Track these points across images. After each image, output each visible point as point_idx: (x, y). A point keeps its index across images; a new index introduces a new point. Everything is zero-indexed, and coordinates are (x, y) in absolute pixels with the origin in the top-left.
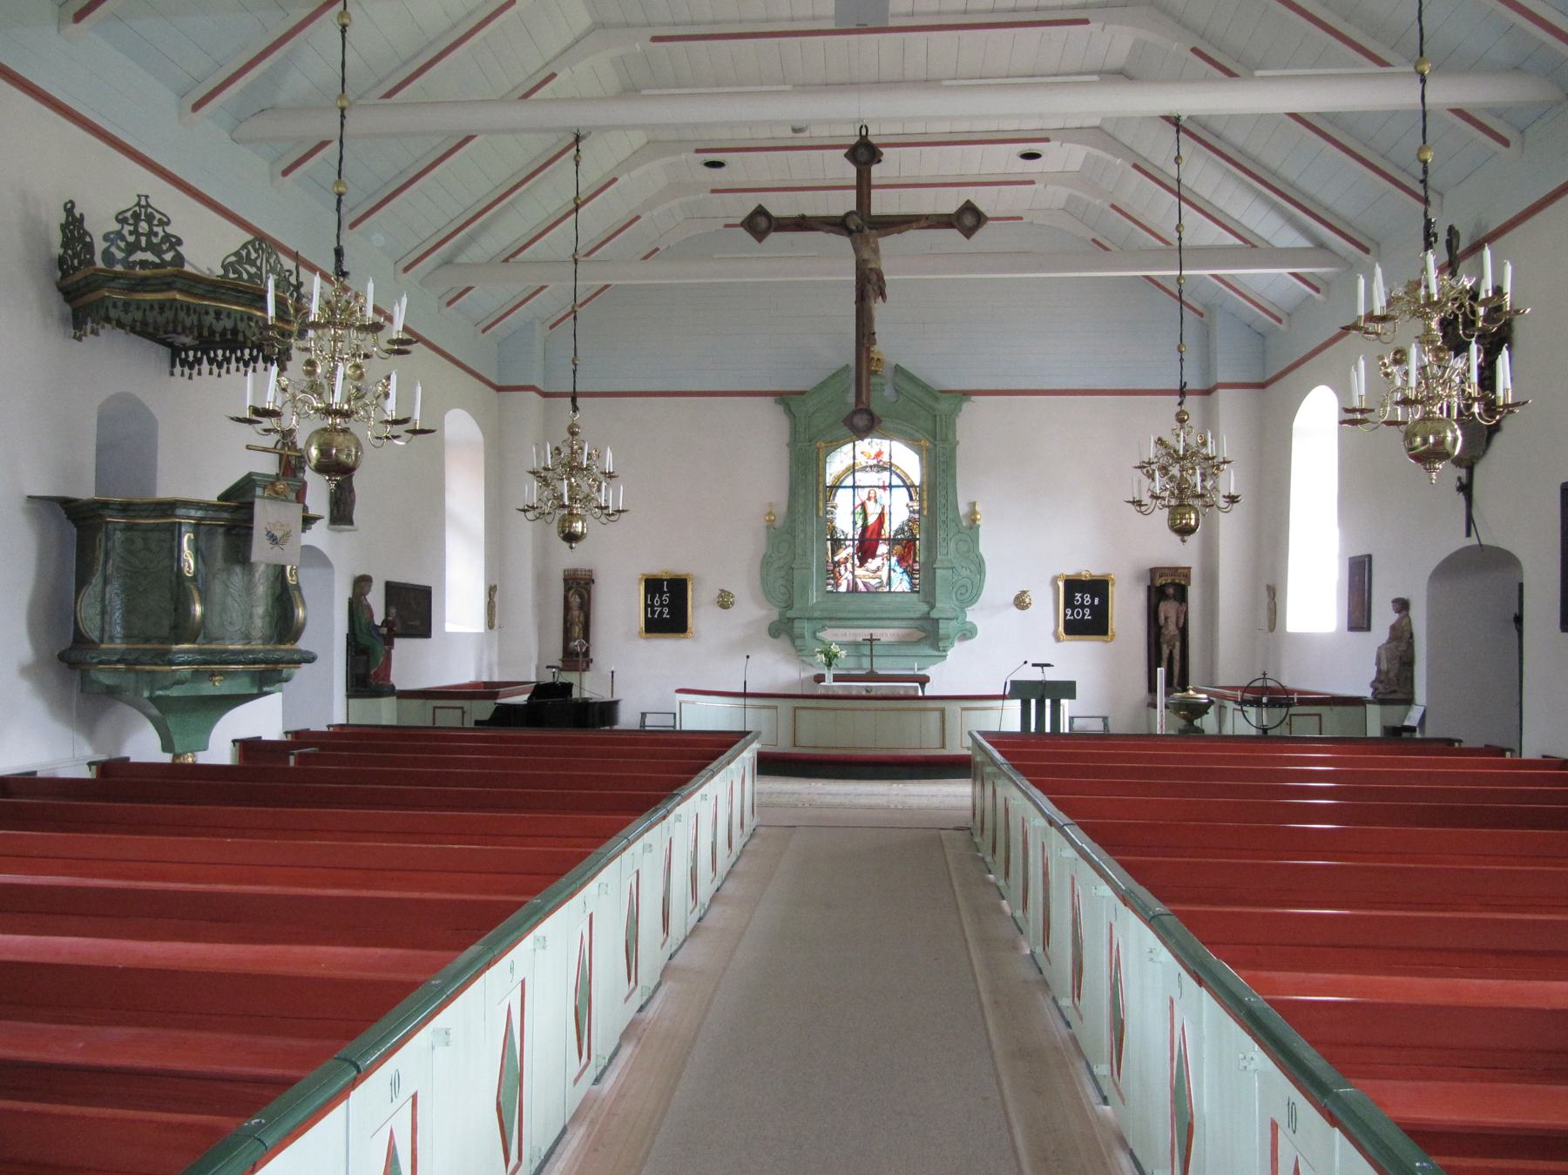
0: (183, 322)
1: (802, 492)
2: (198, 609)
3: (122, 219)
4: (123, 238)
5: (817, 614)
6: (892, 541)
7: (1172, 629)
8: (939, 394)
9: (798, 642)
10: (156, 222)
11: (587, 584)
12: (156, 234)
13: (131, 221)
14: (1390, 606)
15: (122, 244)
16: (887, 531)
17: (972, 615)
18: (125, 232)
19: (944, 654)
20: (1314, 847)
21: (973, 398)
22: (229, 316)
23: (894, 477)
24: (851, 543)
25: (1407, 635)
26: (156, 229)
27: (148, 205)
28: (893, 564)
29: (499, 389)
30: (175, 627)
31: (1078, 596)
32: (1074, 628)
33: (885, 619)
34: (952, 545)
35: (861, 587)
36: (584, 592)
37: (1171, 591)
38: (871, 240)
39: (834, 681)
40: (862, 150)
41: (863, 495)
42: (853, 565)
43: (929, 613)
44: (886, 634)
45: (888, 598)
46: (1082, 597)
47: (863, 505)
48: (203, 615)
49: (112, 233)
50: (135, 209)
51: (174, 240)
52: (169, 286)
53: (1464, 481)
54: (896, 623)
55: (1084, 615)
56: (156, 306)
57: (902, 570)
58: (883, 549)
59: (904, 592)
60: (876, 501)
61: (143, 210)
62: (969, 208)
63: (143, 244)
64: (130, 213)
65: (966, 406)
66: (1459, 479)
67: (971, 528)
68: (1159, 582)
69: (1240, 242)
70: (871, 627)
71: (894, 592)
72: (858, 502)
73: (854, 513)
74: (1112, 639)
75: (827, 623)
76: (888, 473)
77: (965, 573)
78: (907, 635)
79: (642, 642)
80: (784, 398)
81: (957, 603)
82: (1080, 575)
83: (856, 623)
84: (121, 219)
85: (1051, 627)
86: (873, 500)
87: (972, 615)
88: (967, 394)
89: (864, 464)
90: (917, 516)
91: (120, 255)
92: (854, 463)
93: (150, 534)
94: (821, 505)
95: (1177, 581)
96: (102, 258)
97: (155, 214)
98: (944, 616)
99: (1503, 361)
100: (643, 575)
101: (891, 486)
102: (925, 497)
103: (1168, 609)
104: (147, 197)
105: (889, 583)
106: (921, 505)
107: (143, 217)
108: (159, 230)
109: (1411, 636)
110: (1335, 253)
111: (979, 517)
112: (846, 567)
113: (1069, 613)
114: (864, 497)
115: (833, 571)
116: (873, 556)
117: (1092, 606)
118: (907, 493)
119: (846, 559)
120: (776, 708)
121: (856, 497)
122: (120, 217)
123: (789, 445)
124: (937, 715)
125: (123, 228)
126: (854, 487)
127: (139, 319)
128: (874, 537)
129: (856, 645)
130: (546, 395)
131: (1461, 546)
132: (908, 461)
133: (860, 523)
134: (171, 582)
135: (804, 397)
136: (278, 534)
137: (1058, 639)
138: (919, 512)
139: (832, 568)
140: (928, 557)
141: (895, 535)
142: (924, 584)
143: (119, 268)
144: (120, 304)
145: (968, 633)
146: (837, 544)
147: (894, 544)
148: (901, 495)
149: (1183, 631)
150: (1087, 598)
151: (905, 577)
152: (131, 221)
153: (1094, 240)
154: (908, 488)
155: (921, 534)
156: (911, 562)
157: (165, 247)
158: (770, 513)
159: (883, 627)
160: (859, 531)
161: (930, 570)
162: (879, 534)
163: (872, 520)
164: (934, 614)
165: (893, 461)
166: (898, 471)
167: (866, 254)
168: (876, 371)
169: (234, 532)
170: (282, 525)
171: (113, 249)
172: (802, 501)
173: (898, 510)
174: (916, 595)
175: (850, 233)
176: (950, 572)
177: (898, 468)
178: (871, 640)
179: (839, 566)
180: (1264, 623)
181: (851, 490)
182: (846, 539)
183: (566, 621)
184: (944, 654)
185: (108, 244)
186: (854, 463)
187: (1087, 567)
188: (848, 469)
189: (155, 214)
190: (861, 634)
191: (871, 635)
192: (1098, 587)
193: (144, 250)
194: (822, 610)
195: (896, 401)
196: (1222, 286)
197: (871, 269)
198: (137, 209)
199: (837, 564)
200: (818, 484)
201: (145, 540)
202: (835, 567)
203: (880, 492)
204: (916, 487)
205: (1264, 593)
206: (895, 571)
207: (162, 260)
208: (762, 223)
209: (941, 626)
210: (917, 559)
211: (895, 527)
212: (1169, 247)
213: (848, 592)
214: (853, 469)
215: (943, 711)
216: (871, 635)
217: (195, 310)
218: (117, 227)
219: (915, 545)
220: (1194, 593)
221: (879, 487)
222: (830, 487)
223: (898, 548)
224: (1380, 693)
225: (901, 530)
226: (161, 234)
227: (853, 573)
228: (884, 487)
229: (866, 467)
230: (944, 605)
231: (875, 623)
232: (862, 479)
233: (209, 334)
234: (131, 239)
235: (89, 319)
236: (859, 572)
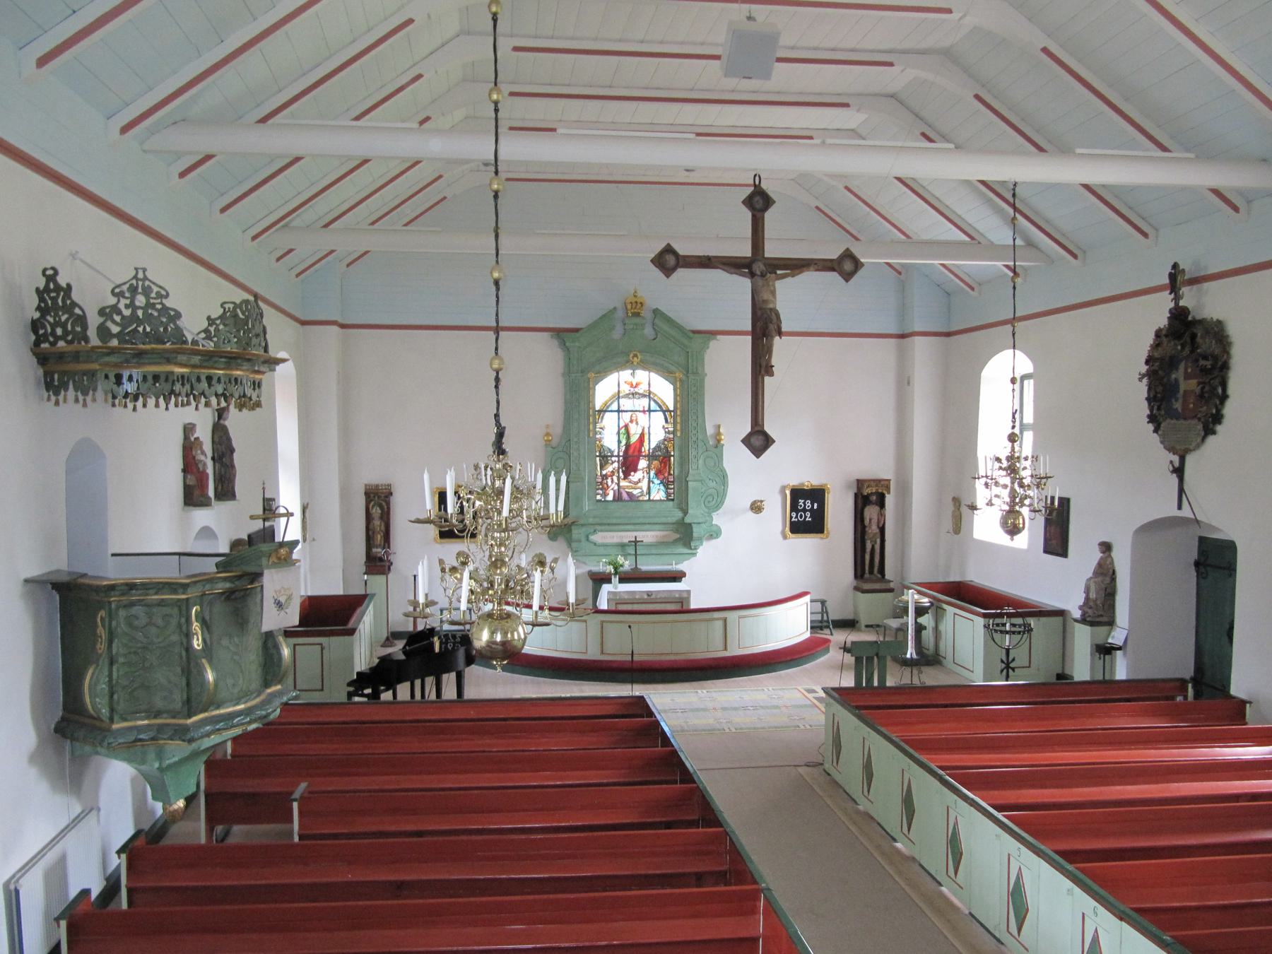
1: (576, 416)
2: (210, 676)
4: (119, 313)
5: (591, 520)
6: (651, 457)
7: (873, 529)
8: (691, 335)
9: (574, 545)
10: (153, 295)
11: (387, 497)
13: (127, 295)
14: (1097, 548)
15: (117, 318)
16: (647, 448)
17: (717, 519)
18: (121, 306)
19: (694, 552)
21: (719, 337)
23: (653, 404)
24: (617, 459)
25: (1111, 571)
27: (145, 278)
28: (652, 476)
29: (304, 323)
30: (188, 701)
31: (801, 502)
32: (797, 528)
33: (645, 524)
34: (701, 462)
35: (625, 496)
36: (384, 504)
37: (874, 498)
38: (771, 283)
40: (757, 198)
41: (626, 417)
42: (619, 478)
43: (683, 519)
44: (648, 536)
45: (649, 504)
46: (804, 503)
47: (626, 426)
48: (216, 681)
49: (108, 307)
50: (131, 282)
51: (172, 313)
52: (168, 358)
53: (1177, 464)
54: (657, 527)
55: (806, 517)
57: (659, 482)
58: (643, 463)
59: (661, 500)
60: (637, 423)
61: (140, 283)
62: (848, 255)
64: (127, 285)
65: (712, 344)
66: (1171, 462)
67: (716, 447)
68: (866, 491)
69: (967, 239)
70: (633, 531)
71: (653, 500)
72: (622, 424)
73: (618, 433)
74: (827, 537)
75: (597, 527)
76: (648, 400)
77: (712, 484)
78: (664, 536)
79: (438, 546)
80: (561, 334)
81: (706, 510)
82: (803, 484)
83: (622, 527)
85: (780, 527)
86: (634, 423)
87: (717, 519)
88: (714, 333)
89: (628, 392)
90: (671, 436)
91: (115, 329)
92: (619, 391)
93: (155, 610)
94: (591, 426)
95: (880, 491)
96: (98, 334)
97: (153, 286)
98: (695, 521)
100: (438, 488)
101: (650, 411)
102: (679, 420)
103: (871, 512)
104: (144, 270)
105: (649, 493)
106: (675, 427)
107: (140, 290)
109: (1114, 572)
110: (1042, 252)
111: (723, 437)
112: (612, 479)
113: (794, 516)
114: (627, 421)
115: (601, 483)
116: (635, 470)
117: (812, 510)
118: (663, 417)
119: (612, 472)
120: (585, 621)
121: (621, 420)
122: (117, 290)
123: (563, 375)
124: (719, 624)
125: (119, 301)
126: (619, 411)
128: (636, 453)
129: (622, 546)
130: (343, 326)
131: (1171, 515)
132: (665, 390)
133: (624, 442)
134: (181, 657)
135: (577, 335)
136: (282, 599)
137: (785, 537)
138: (674, 433)
139: (600, 480)
140: (681, 472)
141: (653, 452)
142: (679, 493)
143: (115, 343)
145: (714, 534)
146: (605, 458)
147: (653, 460)
148: (658, 418)
149: (882, 530)
150: (808, 503)
151: (662, 487)
152: (127, 295)
153: (817, 208)
154: (664, 412)
155: (676, 449)
156: (666, 475)
158: (548, 434)
159: (643, 531)
160: (623, 448)
161: (683, 481)
162: (640, 451)
163: (634, 439)
164: (687, 520)
165: (651, 390)
166: (655, 398)
167: (766, 296)
168: (639, 313)
169: (233, 597)
170: (285, 590)
171: (109, 324)
172: (576, 424)
173: (656, 430)
174: (671, 503)
175: (752, 275)
176: (699, 484)
177: (656, 395)
178: (636, 542)
179: (607, 478)
180: (948, 524)
181: (491, 335)
182: (612, 456)
183: (368, 529)
184: (694, 552)
186: (619, 391)
187: (808, 478)
188: (613, 397)
189: (153, 286)
190: (627, 537)
191: (636, 537)
192: (817, 495)
194: (594, 517)
195: (654, 339)
196: (946, 272)
197: (771, 309)
198: (134, 282)
199: (605, 477)
200: (589, 408)
201: (150, 615)
202: (603, 479)
203: (640, 415)
204: (670, 411)
205: (950, 507)
206: (653, 483)
208: (671, 260)
209: (694, 530)
210: (672, 472)
211: (653, 445)
212: (909, 240)
213: (614, 500)
214: (618, 396)
215: (725, 620)
216: (636, 537)
218: (113, 301)
219: (670, 460)
220: (890, 500)
221: (639, 411)
222: (598, 411)
223: (656, 463)
224: (1089, 616)
225: (658, 448)
227: (618, 484)
228: (644, 411)
229: (629, 394)
230: (695, 514)
231: (637, 527)
232: (626, 404)
234: (127, 313)
236: (623, 483)
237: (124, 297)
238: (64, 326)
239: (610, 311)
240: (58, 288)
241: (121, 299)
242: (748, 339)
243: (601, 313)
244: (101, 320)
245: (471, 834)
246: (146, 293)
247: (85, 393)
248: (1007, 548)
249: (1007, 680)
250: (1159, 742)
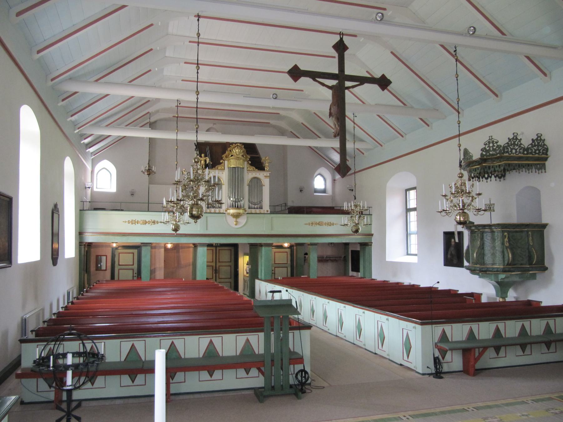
12: (495, 146)
18: (486, 147)
20: (104, 283)
22: (512, 165)
26: (494, 145)
27: (492, 139)
39: (352, 251)
56: (517, 165)
63: (491, 150)
84: (485, 144)
99: (273, 367)
104: (492, 136)
107: (491, 142)
108: (495, 145)
125: (485, 146)
144: (487, 167)
152: (488, 144)
157: (497, 149)
189: (494, 140)
207: (496, 153)
217: (522, 165)
218: (484, 146)
235: (207, 168)
237: (487, 145)
238: (516, 150)
240: (541, 139)
242: (301, 331)
244: (482, 152)
246: (493, 142)
247: (539, 170)
249: (162, 215)
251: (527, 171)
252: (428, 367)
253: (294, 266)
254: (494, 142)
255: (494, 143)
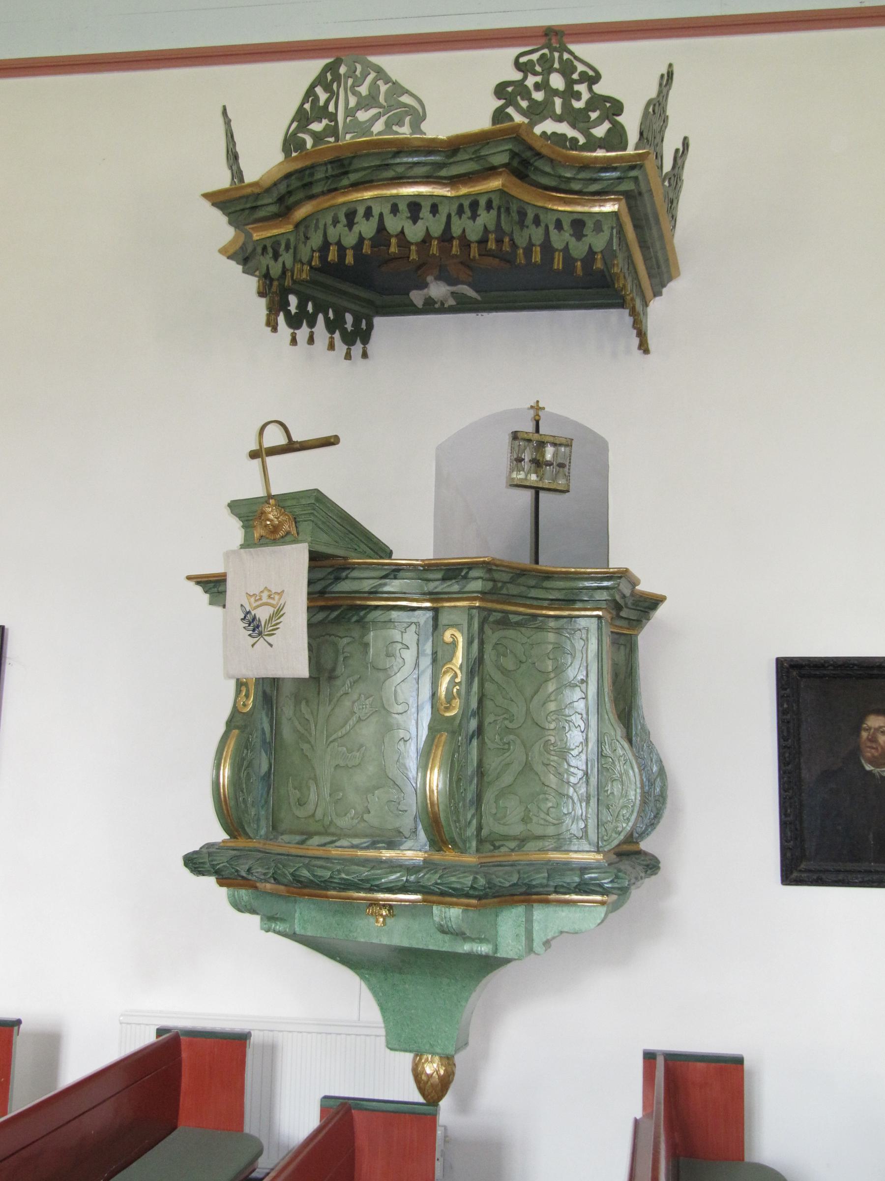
0: (463, 237)
3: (525, 64)
4: (527, 94)
10: (575, 76)
13: (538, 69)
22: (368, 213)
26: (577, 87)
56: (566, 225)
63: (558, 110)
107: (556, 65)
108: (582, 88)
122: (523, 60)
125: (525, 78)
127: (436, 235)
157: (594, 115)
171: (510, 110)
185: (502, 102)
189: (576, 63)
193: (559, 119)
218: (517, 76)
224: (570, 735)
226: (586, 96)
233: (452, 241)
239: (385, 970)
241: (529, 75)
243: (327, 857)
244: (501, 102)
245: (261, 604)
248: (435, 1159)
250: (316, 1134)
251: (341, 347)
252: (271, 645)
253: (584, 196)
254: (575, 68)
255: (575, 76)
